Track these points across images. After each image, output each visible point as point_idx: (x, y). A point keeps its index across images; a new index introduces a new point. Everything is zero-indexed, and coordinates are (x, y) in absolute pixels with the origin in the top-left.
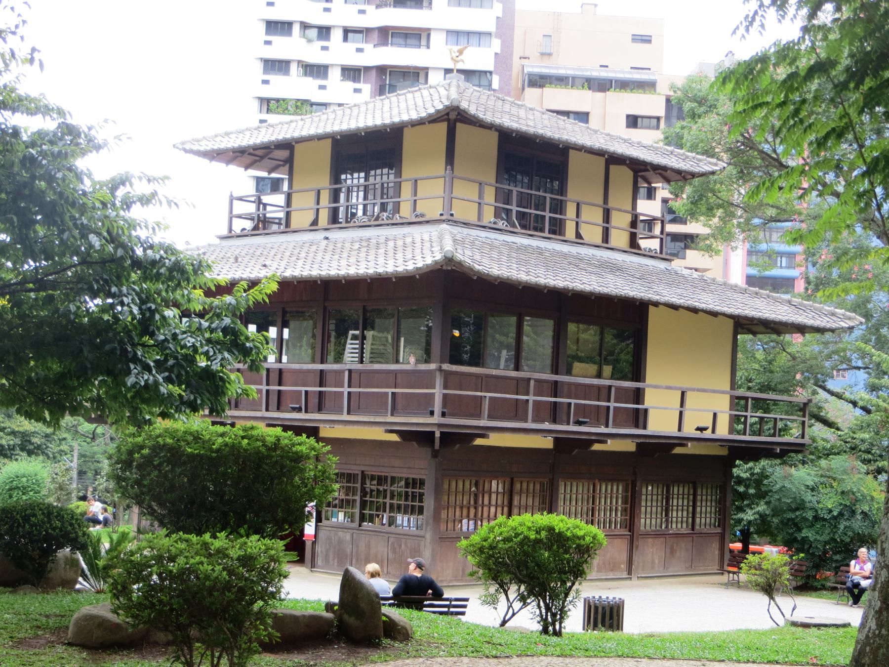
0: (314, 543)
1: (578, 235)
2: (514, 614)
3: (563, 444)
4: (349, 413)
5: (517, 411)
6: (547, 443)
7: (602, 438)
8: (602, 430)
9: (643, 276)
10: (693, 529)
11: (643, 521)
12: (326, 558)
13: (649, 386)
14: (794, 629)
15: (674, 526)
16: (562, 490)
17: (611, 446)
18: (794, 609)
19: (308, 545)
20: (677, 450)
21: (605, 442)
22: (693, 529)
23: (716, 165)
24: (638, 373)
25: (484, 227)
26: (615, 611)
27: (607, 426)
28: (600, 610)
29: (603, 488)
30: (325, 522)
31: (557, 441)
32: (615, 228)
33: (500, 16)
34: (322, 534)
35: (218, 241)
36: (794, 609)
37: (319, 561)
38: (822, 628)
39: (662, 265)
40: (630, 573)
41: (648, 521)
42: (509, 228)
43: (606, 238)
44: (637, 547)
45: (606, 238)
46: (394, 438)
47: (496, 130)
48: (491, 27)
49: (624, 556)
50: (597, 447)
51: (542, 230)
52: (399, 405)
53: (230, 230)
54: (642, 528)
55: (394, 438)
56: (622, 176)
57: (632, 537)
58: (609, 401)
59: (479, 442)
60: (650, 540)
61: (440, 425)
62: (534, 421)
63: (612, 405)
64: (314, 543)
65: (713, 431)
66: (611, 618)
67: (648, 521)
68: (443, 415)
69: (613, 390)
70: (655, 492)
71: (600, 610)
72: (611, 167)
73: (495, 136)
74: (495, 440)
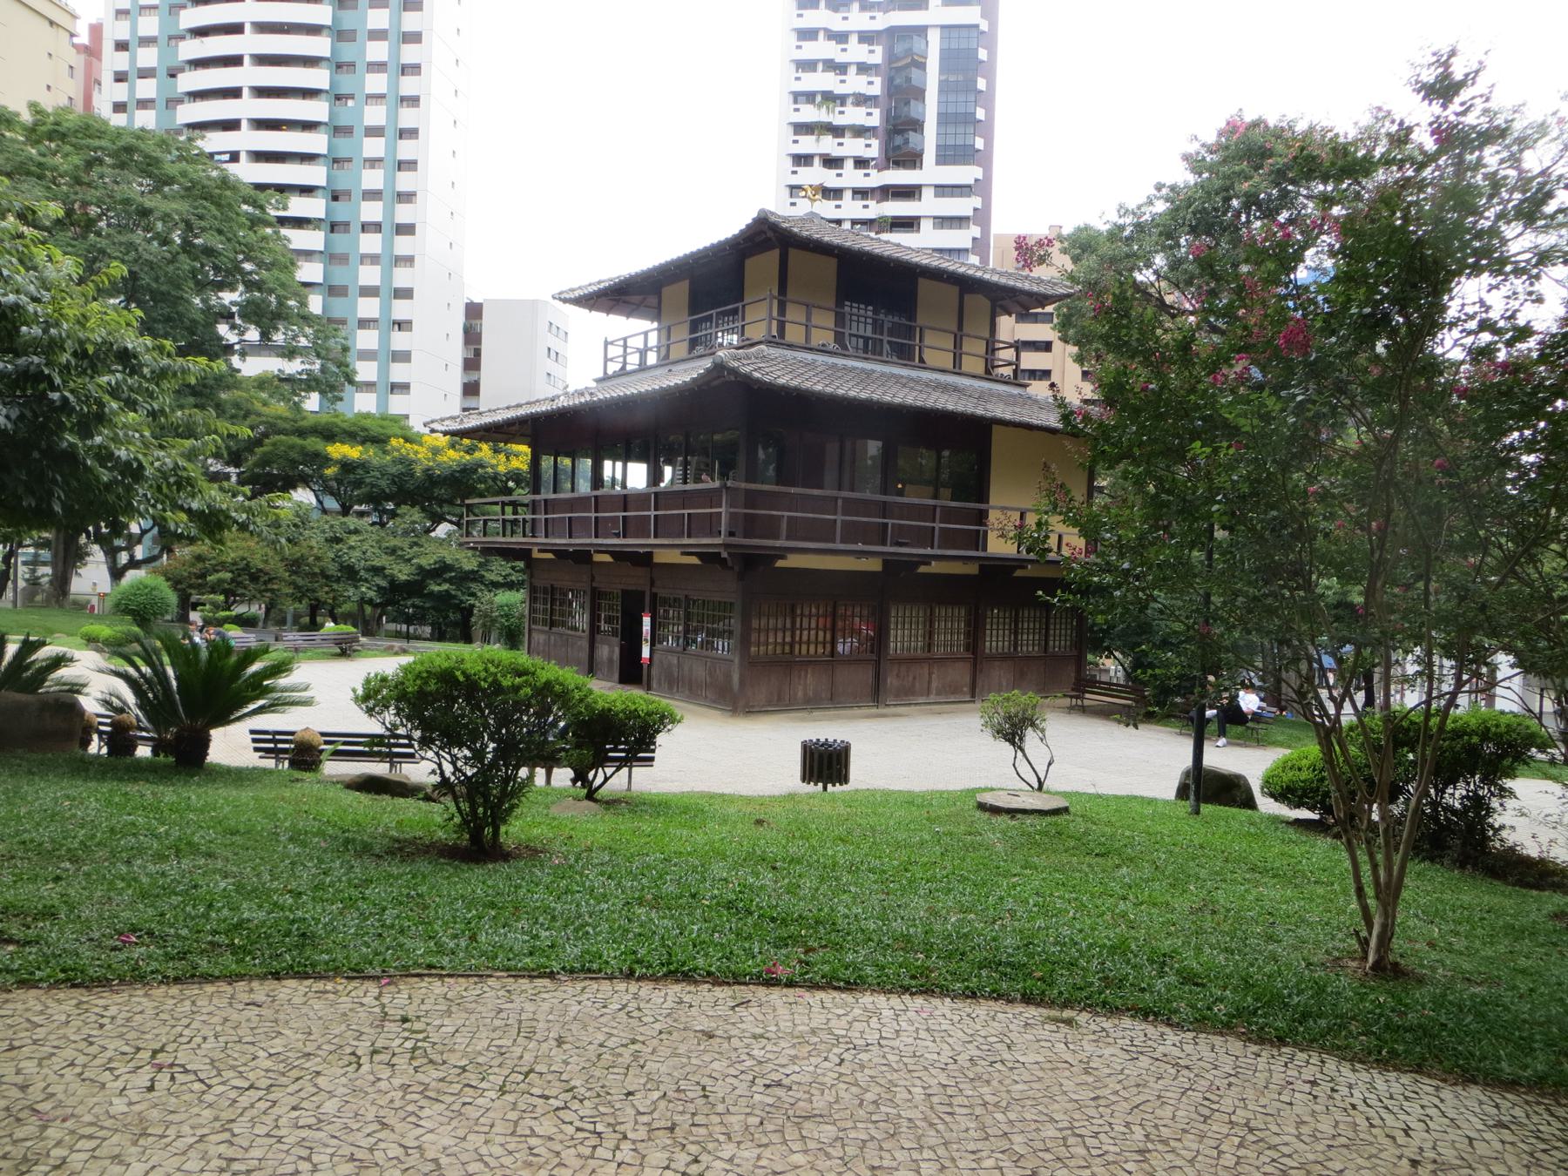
0: (650, 666)
1: (922, 360)
2: (606, 779)
3: (890, 564)
4: (656, 536)
5: (822, 532)
6: (874, 565)
7: (926, 560)
8: (929, 551)
9: (982, 397)
10: (1046, 651)
11: (988, 644)
12: (659, 683)
13: (993, 508)
14: (978, 814)
15: (1025, 648)
16: (893, 613)
17: (935, 567)
18: (1050, 764)
19: (645, 667)
20: (1019, 573)
21: (929, 564)
22: (1046, 651)
23: (1072, 288)
24: (983, 496)
25: (811, 349)
26: (835, 758)
27: (932, 548)
28: (816, 756)
29: (941, 611)
30: (658, 646)
31: (886, 563)
32: (967, 354)
33: (978, 236)
34: (656, 657)
35: (594, 384)
36: (1050, 764)
37: (654, 685)
38: (1019, 816)
39: (1016, 391)
40: (973, 696)
41: (994, 644)
42: (840, 351)
43: (957, 361)
44: (981, 671)
45: (957, 361)
46: (694, 560)
47: (836, 256)
48: (969, 245)
49: (967, 679)
50: (922, 569)
51: (881, 354)
52: (549, 508)
53: (605, 373)
54: (987, 651)
55: (694, 560)
56: (980, 302)
57: (975, 659)
58: (934, 521)
59: (922, 569)
60: (997, 663)
61: (726, 546)
62: (842, 541)
63: (938, 525)
64: (650, 666)
65: (573, 490)
66: (830, 767)
67: (994, 644)
68: (731, 534)
69: (938, 510)
70: (1001, 615)
71: (816, 756)
72: (967, 297)
73: (831, 264)
74: (793, 561)
